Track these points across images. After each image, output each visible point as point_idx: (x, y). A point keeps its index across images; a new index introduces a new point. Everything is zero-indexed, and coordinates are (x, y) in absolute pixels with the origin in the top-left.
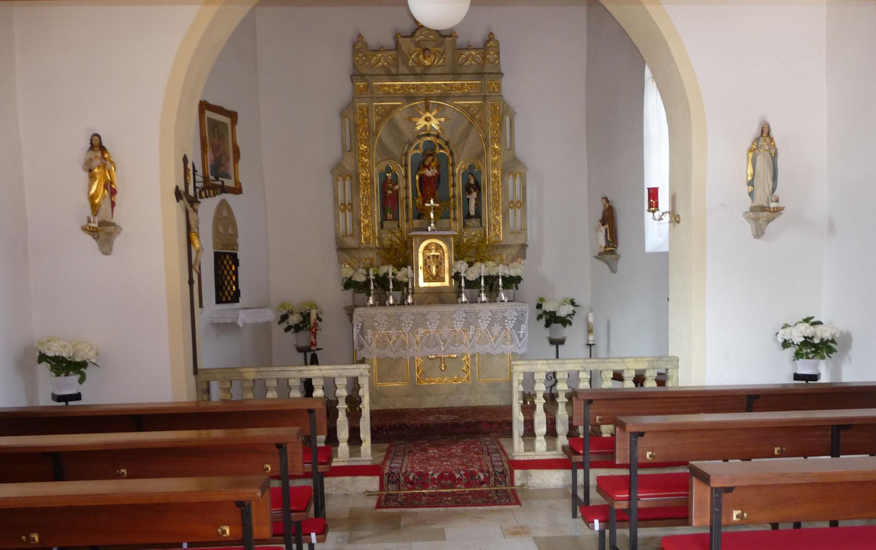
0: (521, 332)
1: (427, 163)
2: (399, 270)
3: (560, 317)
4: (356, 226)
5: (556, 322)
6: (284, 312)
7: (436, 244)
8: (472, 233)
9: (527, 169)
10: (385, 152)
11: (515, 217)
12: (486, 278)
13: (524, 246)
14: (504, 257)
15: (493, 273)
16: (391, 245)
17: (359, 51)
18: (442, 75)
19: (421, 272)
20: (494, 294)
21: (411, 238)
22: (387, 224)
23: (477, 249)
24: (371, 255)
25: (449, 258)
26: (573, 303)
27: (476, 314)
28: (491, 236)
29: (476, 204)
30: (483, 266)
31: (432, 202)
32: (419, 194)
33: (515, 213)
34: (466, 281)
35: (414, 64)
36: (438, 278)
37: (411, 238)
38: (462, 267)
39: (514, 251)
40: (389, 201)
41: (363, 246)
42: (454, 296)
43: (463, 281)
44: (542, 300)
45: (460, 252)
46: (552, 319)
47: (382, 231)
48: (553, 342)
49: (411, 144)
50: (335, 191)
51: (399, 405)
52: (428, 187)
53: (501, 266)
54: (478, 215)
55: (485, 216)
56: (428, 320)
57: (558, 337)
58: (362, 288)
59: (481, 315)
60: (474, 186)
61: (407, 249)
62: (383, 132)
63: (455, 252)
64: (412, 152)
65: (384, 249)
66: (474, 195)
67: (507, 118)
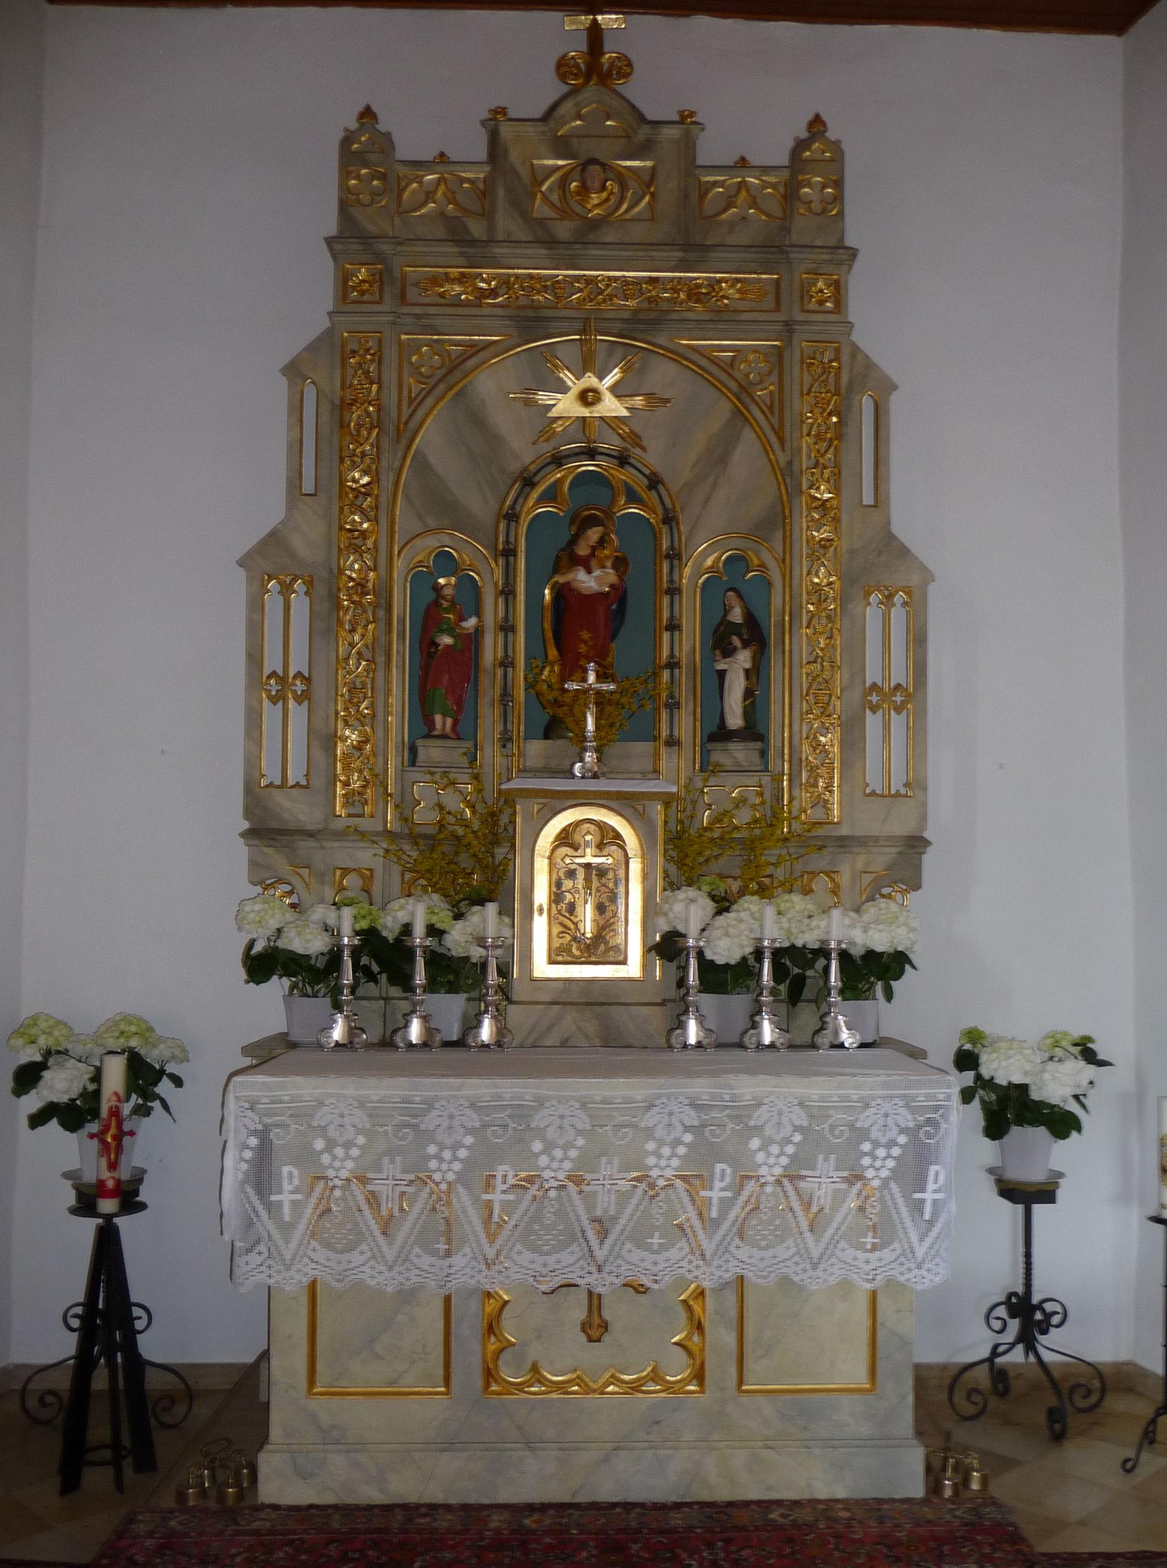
0: (928, 1196)
1: (582, 550)
2: (458, 916)
3: (1041, 1104)
4: (319, 755)
5: (1034, 1123)
6: (32, 1055)
7: (602, 827)
8: (732, 793)
9: (927, 576)
10: (443, 508)
11: (883, 745)
12: (778, 954)
13: (916, 844)
14: (844, 879)
15: (808, 938)
16: (441, 826)
17: (360, 158)
18: (640, 251)
19: (540, 926)
20: (806, 1016)
21: (509, 799)
22: (432, 751)
23: (751, 846)
24: (367, 856)
25: (645, 877)
26: (1089, 1056)
27: (741, 1113)
28: (798, 802)
29: (748, 693)
30: (770, 912)
31: (592, 678)
32: (553, 653)
33: (887, 726)
34: (706, 966)
35: (549, 213)
36: (600, 947)
37: (509, 799)
38: (690, 911)
39: (880, 859)
40: (444, 675)
41: (339, 825)
42: (656, 1019)
43: (693, 963)
44: (974, 1035)
45: (685, 857)
46: (1009, 1110)
47: (414, 774)
48: (1010, 1191)
49: (529, 483)
50: (255, 630)
51: (405, 1487)
52: (577, 629)
53: (836, 914)
54: (754, 731)
55: (779, 733)
56: (540, 1133)
57: (1035, 1175)
58: (311, 974)
59: (760, 1116)
60: (744, 631)
61: (496, 842)
62: (432, 437)
63: (668, 859)
64: (534, 508)
65: (415, 838)
66: (744, 658)
67: (867, 403)
